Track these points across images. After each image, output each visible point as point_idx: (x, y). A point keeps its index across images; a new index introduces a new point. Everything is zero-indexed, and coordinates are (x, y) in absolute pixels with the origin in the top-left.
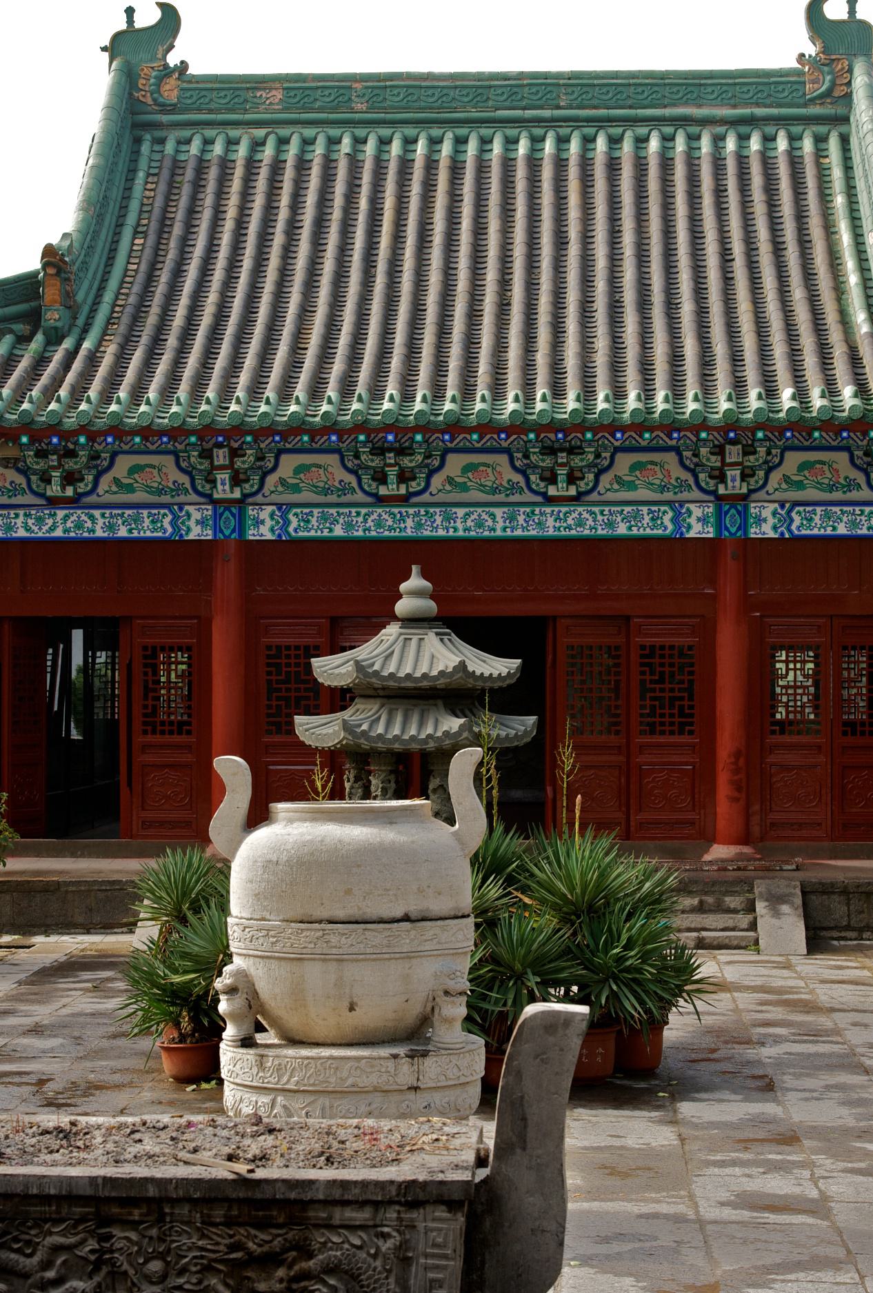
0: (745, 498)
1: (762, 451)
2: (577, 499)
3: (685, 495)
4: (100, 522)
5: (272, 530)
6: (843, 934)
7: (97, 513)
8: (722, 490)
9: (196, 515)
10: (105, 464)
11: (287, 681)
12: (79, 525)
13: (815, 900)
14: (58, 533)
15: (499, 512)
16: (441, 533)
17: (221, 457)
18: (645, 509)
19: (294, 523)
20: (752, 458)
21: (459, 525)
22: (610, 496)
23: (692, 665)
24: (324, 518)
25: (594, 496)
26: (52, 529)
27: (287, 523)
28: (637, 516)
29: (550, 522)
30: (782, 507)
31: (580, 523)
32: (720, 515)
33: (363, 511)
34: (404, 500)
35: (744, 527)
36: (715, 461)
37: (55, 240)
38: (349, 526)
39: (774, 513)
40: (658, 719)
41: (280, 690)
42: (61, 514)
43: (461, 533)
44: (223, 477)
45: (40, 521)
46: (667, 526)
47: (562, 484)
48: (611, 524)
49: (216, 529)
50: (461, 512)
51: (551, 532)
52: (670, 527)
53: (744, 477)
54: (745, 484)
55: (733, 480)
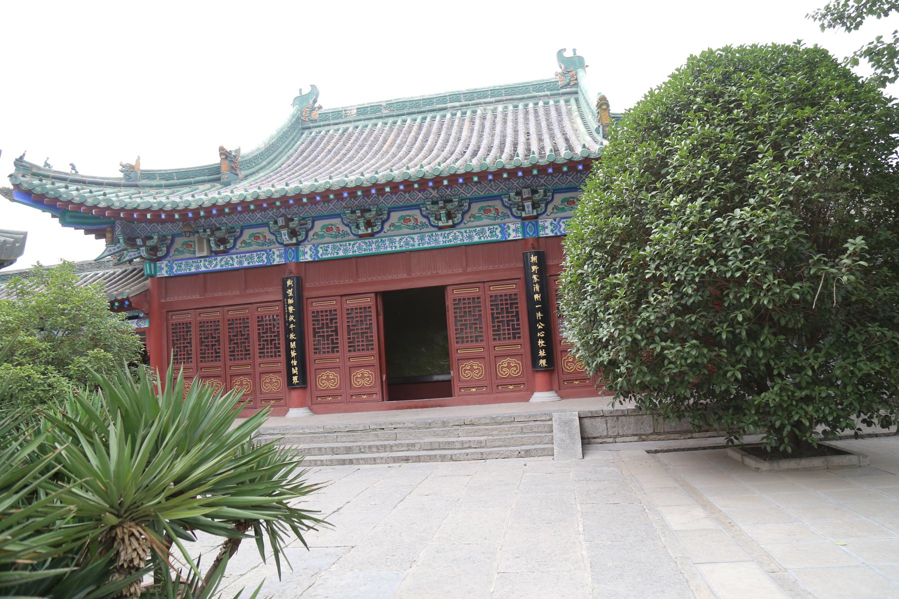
0: (536, 217)
1: (541, 191)
2: (454, 226)
3: (507, 220)
4: (236, 260)
5: (311, 256)
6: (605, 440)
7: (234, 256)
8: (524, 215)
9: (277, 253)
10: (385, 217)
11: (322, 328)
12: (227, 263)
13: (587, 422)
14: (218, 267)
15: (416, 237)
16: (389, 249)
17: (526, 193)
18: (487, 228)
19: (321, 251)
20: (537, 195)
21: (397, 245)
22: (389, 233)
23: (517, 303)
24: (187, 265)
25: (234, 251)
26: (215, 266)
27: (317, 252)
28: (483, 232)
29: (441, 239)
30: (555, 220)
31: (455, 238)
32: (524, 227)
33: (352, 243)
34: (372, 235)
35: (536, 231)
36: (518, 199)
37: (697, 54)
38: (345, 250)
39: (551, 224)
40: (474, 335)
41: (498, 318)
42: (219, 258)
43: (398, 249)
44: (528, 204)
45: (210, 263)
46: (264, 261)
47: (363, 228)
48: (470, 237)
49: (286, 258)
50: (398, 238)
51: (441, 244)
52: (500, 235)
53: (534, 208)
54: (535, 211)
55: (528, 207)
